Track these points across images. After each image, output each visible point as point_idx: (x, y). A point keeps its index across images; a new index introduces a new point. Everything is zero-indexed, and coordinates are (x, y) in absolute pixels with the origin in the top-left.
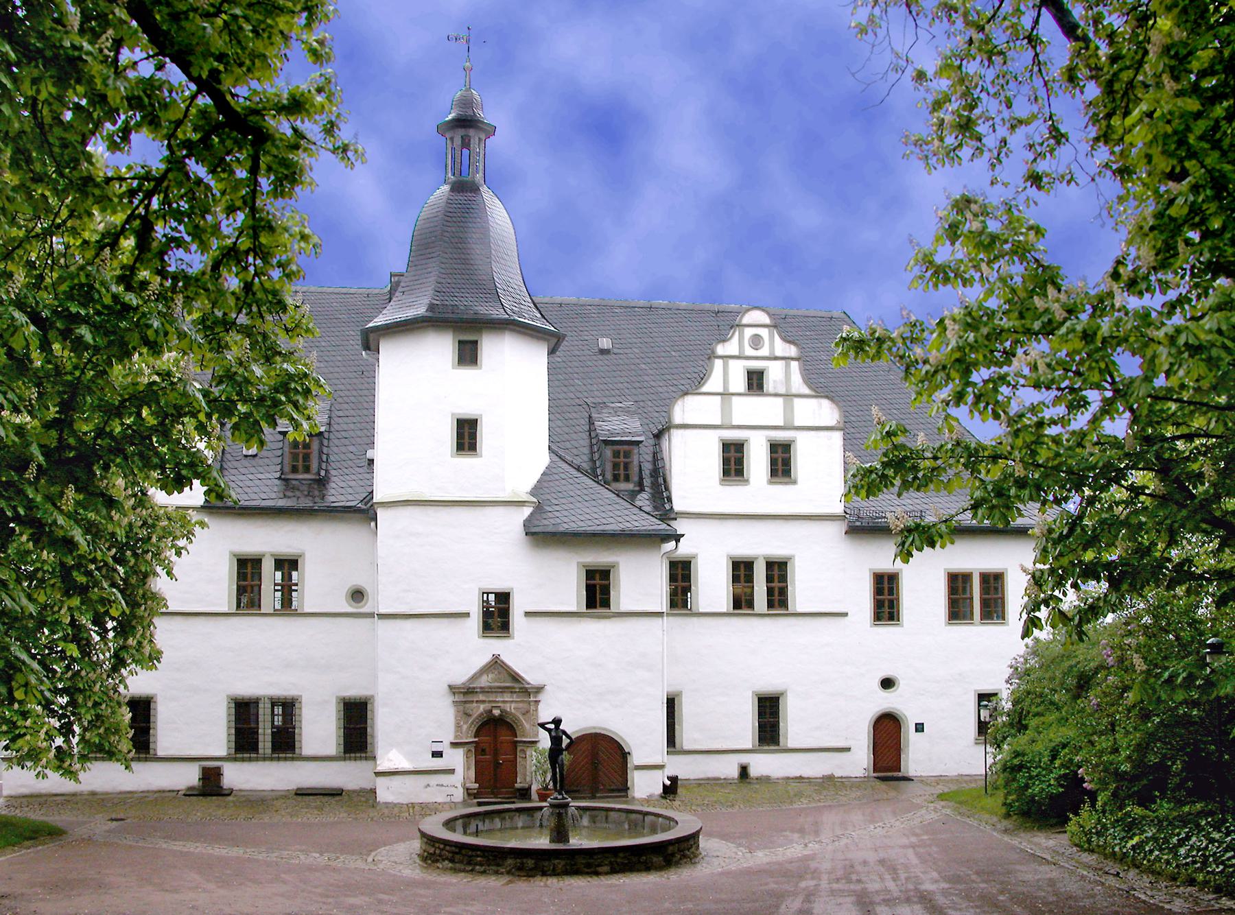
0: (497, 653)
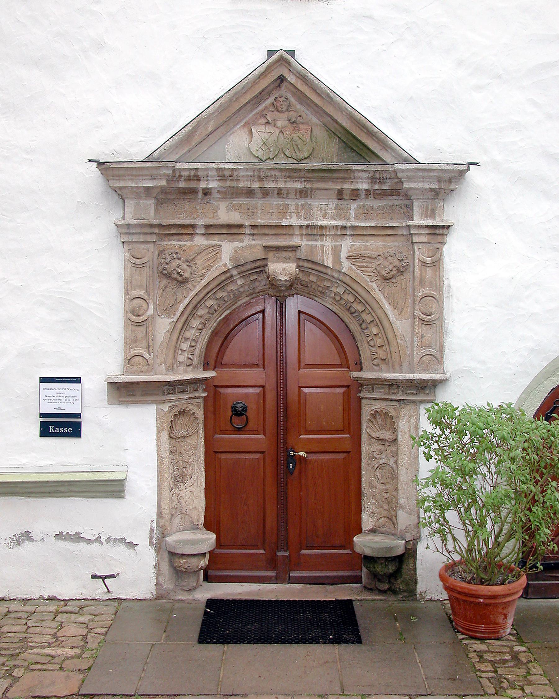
0: (282, 44)
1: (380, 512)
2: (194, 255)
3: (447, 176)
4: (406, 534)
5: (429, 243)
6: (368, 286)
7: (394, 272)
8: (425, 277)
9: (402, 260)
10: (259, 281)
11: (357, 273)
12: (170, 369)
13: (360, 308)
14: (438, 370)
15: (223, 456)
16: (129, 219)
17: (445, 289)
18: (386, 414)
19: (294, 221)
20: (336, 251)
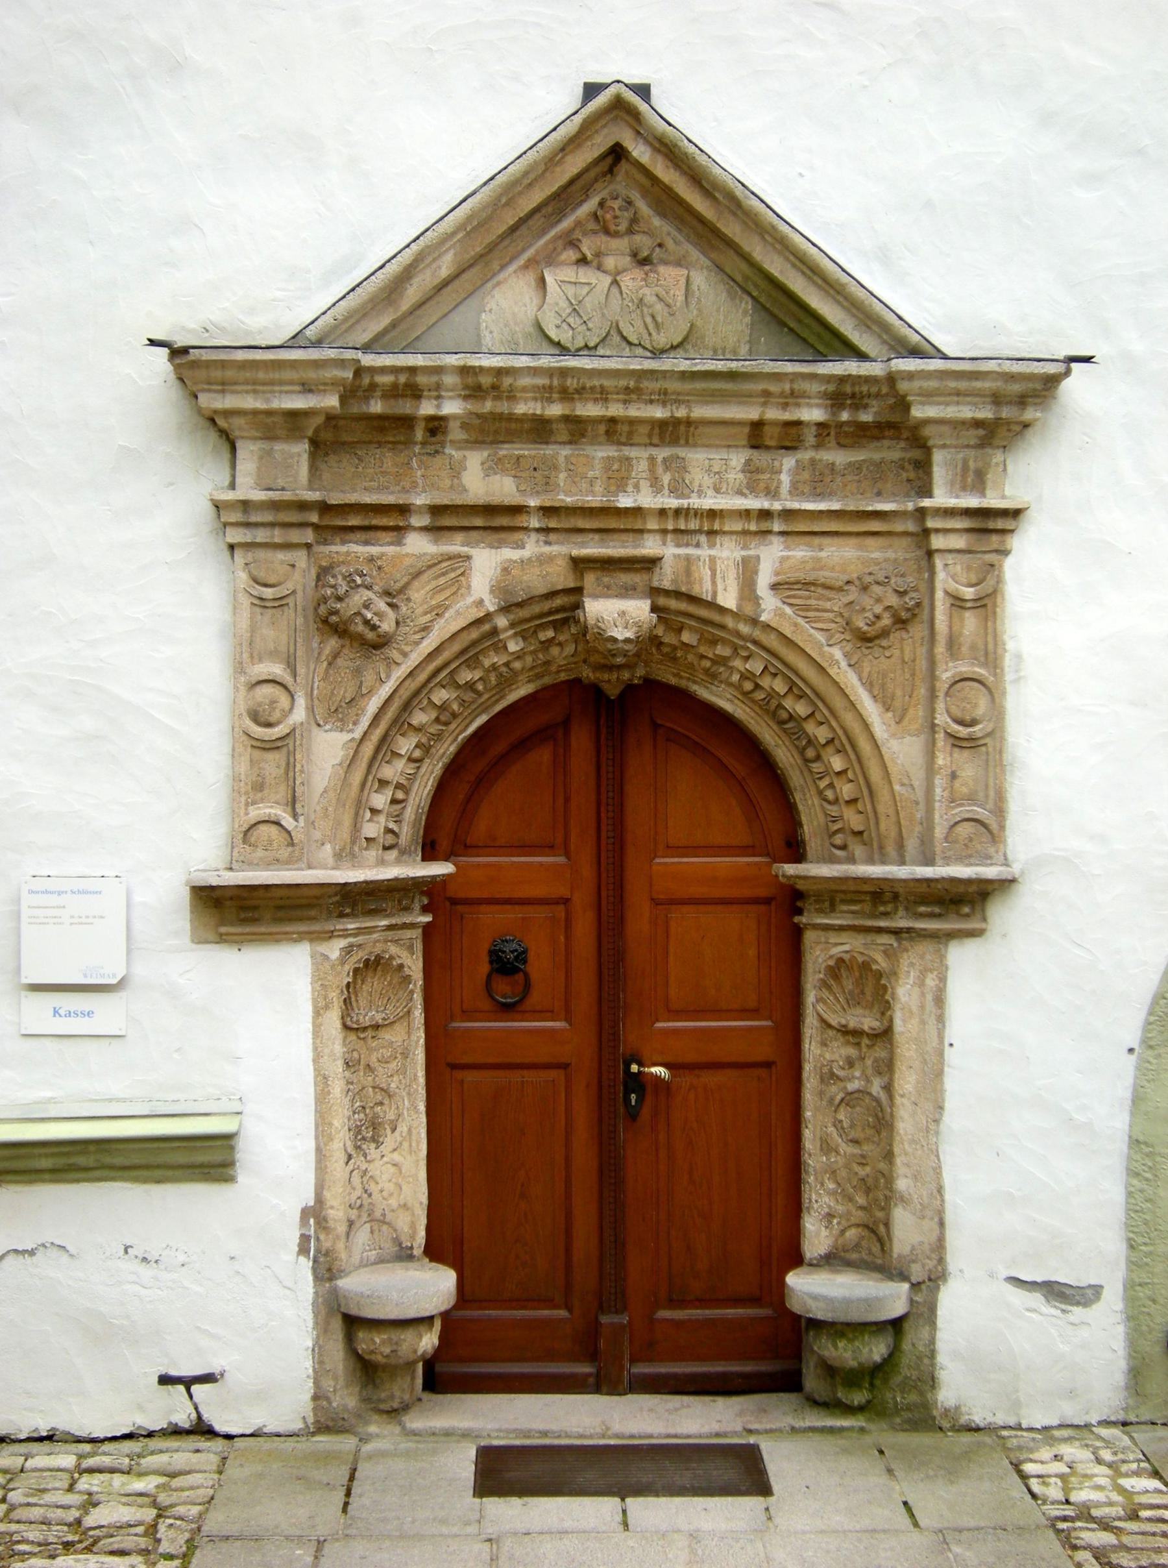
0: (619, 67)
1: (849, 1213)
2: (405, 580)
3: (1016, 388)
4: (913, 1265)
5: (970, 552)
6: (822, 654)
7: (886, 621)
8: (961, 634)
9: (905, 593)
10: (560, 644)
11: (796, 625)
12: (344, 856)
13: (801, 709)
14: (990, 858)
15: (471, 1077)
16: (249, 490)
17: (1008, 661)
18: (866, 966)
19: (647, 499)
20: (748, 571)
